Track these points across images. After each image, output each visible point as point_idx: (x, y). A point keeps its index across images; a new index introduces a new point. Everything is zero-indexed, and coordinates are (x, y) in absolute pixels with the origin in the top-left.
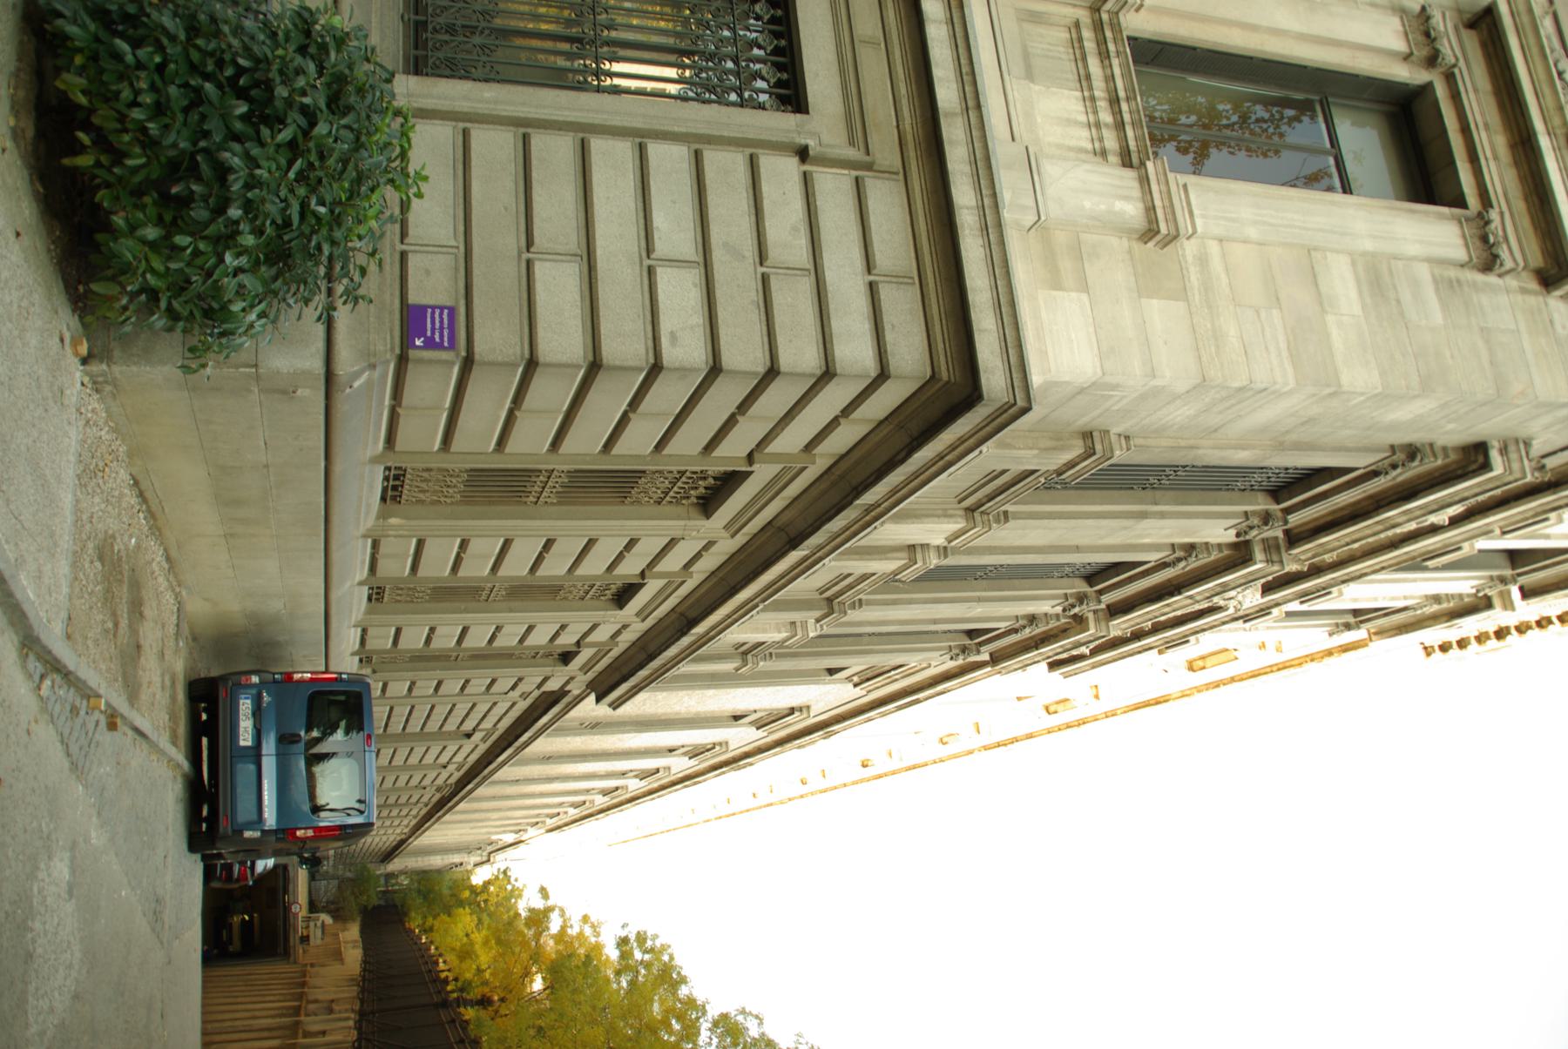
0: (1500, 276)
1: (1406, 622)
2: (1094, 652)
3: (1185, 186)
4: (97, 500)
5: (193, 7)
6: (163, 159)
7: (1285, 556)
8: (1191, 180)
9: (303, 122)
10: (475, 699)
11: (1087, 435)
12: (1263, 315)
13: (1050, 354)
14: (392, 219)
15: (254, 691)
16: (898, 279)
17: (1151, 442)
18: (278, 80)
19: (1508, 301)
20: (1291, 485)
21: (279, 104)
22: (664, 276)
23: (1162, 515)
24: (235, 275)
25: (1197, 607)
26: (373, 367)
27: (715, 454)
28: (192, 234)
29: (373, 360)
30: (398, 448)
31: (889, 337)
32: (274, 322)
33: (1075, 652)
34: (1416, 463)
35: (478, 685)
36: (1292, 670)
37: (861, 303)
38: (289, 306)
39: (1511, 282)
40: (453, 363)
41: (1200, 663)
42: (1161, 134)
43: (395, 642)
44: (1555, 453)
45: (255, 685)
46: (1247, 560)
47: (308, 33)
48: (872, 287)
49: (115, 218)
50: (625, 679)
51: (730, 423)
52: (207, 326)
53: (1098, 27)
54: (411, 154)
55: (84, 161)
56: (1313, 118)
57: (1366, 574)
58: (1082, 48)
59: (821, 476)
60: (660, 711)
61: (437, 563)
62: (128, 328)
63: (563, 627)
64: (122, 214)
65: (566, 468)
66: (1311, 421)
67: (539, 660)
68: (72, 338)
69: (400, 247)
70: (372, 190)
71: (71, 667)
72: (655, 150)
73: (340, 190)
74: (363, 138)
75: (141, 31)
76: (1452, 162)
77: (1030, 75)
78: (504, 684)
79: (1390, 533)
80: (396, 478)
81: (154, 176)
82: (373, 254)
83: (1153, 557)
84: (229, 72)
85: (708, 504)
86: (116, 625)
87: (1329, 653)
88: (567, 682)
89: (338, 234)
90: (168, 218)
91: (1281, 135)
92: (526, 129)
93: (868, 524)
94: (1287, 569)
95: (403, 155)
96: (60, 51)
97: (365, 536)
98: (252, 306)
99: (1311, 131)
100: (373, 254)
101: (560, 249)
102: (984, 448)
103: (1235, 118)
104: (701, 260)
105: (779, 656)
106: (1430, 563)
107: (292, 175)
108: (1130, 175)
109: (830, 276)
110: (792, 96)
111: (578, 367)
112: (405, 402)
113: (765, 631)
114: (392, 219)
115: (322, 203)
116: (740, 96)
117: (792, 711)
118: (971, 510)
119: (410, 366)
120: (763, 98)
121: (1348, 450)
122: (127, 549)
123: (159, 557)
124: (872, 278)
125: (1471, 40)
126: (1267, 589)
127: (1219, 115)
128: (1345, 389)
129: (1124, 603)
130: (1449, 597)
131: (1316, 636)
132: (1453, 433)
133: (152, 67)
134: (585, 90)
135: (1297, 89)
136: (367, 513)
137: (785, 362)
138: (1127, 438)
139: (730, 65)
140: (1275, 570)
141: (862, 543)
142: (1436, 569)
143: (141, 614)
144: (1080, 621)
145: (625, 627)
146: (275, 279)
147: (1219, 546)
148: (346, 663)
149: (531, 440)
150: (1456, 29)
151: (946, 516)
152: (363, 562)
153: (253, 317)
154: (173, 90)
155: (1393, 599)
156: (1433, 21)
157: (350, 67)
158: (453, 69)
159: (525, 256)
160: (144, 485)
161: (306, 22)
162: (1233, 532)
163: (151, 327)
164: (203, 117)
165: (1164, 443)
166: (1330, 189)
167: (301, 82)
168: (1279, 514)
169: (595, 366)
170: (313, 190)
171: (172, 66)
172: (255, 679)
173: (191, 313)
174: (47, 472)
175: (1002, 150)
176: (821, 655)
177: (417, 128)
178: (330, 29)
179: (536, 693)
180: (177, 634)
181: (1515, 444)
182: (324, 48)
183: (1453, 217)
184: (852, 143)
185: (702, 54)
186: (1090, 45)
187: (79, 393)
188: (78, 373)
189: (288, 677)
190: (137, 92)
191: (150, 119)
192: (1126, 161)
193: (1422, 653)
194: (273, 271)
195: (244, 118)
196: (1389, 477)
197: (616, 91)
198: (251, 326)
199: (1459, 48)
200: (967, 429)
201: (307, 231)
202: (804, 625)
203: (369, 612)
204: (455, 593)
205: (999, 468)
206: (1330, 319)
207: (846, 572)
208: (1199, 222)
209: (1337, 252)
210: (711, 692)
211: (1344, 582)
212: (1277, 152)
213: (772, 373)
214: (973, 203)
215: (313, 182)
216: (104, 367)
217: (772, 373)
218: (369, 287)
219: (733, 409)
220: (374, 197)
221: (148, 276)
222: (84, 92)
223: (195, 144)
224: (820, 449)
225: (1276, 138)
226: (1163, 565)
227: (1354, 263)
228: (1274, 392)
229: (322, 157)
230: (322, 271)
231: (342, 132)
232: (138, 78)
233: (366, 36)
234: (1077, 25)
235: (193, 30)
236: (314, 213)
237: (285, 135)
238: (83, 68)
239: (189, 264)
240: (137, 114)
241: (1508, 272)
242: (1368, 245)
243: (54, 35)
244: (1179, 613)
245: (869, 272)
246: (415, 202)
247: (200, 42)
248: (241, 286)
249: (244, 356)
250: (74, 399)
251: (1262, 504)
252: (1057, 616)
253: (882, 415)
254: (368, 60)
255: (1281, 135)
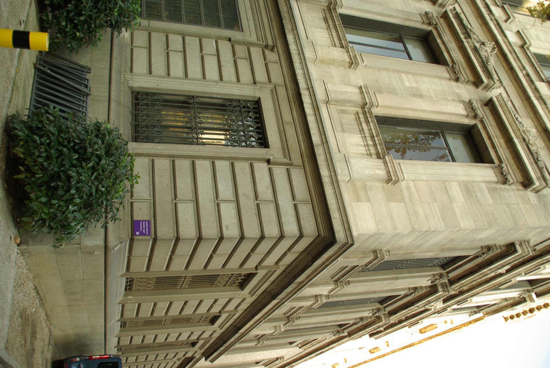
0: (509, 185)
1: (495, 309)
2: (386, 329)
3: (399, 163)
4: (21, 295)
5: (60, 124)
6: (48, 174)
7: (449, 289)
8: (401, 161)
9: (97, 160)
10: (160, 362)
11: (375, 252)
12: (431, 205)
13: (359, 224)
14: (128, 191)
15: (77, 364)
16: (303, 202)
17: (397, 252)
18: (88, 146)
19: (513, 193)
20: (448, 263)
21: (89, 154)
22: (223, 206)
23: (404, 278)
24: (73, 213)
25: (420, 310)
26: (121, 243)
27: (226, 268)
28: (58, 200)
29: (121, 240)
30: (131, 271)
31: (302, 222)
32: (86, 229)
33: (378, 330)
34: (491, 252)
35: (161, 356)
36: (458, 330)
37: (292, 211)
38: (92, 223)
39: (513, 187)
40: (150, 240)
41: (424, 330)
42: (389, 146)
43: (131, 342)
44: (538, 244)
45: (78, 361)
46: (436, 291)
47: (99, 130)
48: (295, 206)
49: (31, 195)
50: (215, 351)
51: (249, 256)
52: (63, 231)
53: (364, 113)
54: (134, 169)
55: (22, 176)
56: (439, 137)
57: (479, 293)
58: (360, 120)
59: (282, 273)
60: (229, 362)
61: (145, 312)
62: (34, 233)
63: (192, 333)
64: (34, 194)
65: (191, 275)
66: (452, 240)
67: (183, 346)
68: (15, 237)
69: (130, 200)
70: (121, 182)
71: (6, 360)
72: (218, 163)
73: (109, 183)
74: (118, 164)
75: (43, 133)
76: (487, 149)
77: (343, 131)
78: (171, 356)
79: (485, 277)
80: (130, 282)
81: (45, 180)
82: (121, 204)
83: (403, 293)
84: (72, 144)
85: (242, 285)
86: (25, 342)
87: (470, 323)
88: (194, 354)
89: (109, 197)
90: (50, 194)
91: (430, 144)
92: (173, 158)
93: (300, 289)
94: (451, 293)
95: (131, 169)
96: (15, 140)
97: (119, 303)
98: (79, 224)
99: (439, 142)
100: (121, 204)
101: (186, 198)
102: (339, 259)
103: (413, 139)
104: (235, 200)
105: (272, 339)
106: (501, 287)
107: (93, 178)
108: (380, 161)
109: (280, 203)
110: (264, 143)
111: (194, 239)
112: (133, 255)
113: (265, 330)
114: (128, 191)
115: (103, 187)
116: (246, 143)
117: (277, 359)
118: (336, 281)
119: (135, 242)
120: (254, 144)
121: (466, 249)
122: (31, 313)
123: (43, 315)
124: (295, 202)
125: (487, 109)
126: (445, 301)
127: (408, 139)
128: (462, 228)
129: (393, 311)
130: (510, 299)
131: (464, 317)
132: (502, 240)
133: (46, 144)
134: (193, 144)
135: (432, 129)
136: (120, 295)
137: (267, 233)
138: (389, 251)
139: (242, 133)
140: (447, 294)
141: (298, 296)
142: (504, 289)
143: (35, 337)
144: (379, 318)
145: (215, 332)
146: (87, 214)
147: (426, 287)
148: (112, 351)
149: (178, 266)
150: (481, 106)
151: (327, 284)
152: (119, 313)
153: (79, 227)
154: (53, 151)
155: (490, 301)
156: (474, 104)
157: (113, 141)
158: (148, 140)
159: (174, 201)
160: (38, 288)
161: (98, 127)
162: (430, 282)
163: (43, 232)
164: (63, 160)
165: (402, 252)
166: (448, 161)
167: (96, 147)
168: (445, 274)
169: (200, 239)
170: (100, 183)
171: (53, 143)
172: (78, 359)
173: (57, 226)
174: (3, 286)
175: (336, 156)
176: (286, 338)
177: (136, 160)
178: (106, 129)
179: (183, 358)
180: (49, 344)
181: (524, 242)
182: (104, 135)
183: (490, 167)
184: (285, 157)
185: (232, 130)
186: (362, 119)
187: (16, 256)
188: (16, 249)
189: (91, 357)
190: (41, 153)
191: (44, 161)
192: (379, 157)
193: (504, 320)
194: (86, 211)
195: (76, 159)
196: (482, 258)
197: (204, 144)
198: (78, 230)
199: (483, 112)
200: (332, 253)
201: (98, 196)
202: (280, 327)
203: (121, 331)
204: (152, 323)
205: (345, 265)
206: (454, 204)
207: (293, 307)
208: (405, 175)
209: (453, 182)
210: (247, 354)
211: (472, 296)
212: (429, 150)
213: (262, 237)
214: (328, 174)
215: (100, 180)
216: (26, 247)
217: (262, 237)
218: (120, 215)
219: (249, 251)
220: (121, 184)
221: (42, 215)
222: (23, 153)
223: (60, 169)
224: (280, 264)
225: (428, 145)
226: (406, 296)
227: (459, 185)
228: (438, 231)
229: (103, 171)
230: (103, 210)
231: (110, 163)
232: (41, 148)
233: (118, 130)
234: (357, 113)
235: (60, 131)
236: (101, 191)
237: (90, 165)
238: (23, 145)
239: (57, 210)
240: (40, 160)
241: (512, 184)
242: (464, 179)
243: (14, 135)
244: (414, 312)
245: (294, 200)
246: (135, 185)
247: (62, 135)
248: (75, 217)
249: (75, 241)
250: (14, 259)
251: (439, 271)
252: (371, 317)
253: (302, 250)
254: (119, 138)
255: (430, 144)
